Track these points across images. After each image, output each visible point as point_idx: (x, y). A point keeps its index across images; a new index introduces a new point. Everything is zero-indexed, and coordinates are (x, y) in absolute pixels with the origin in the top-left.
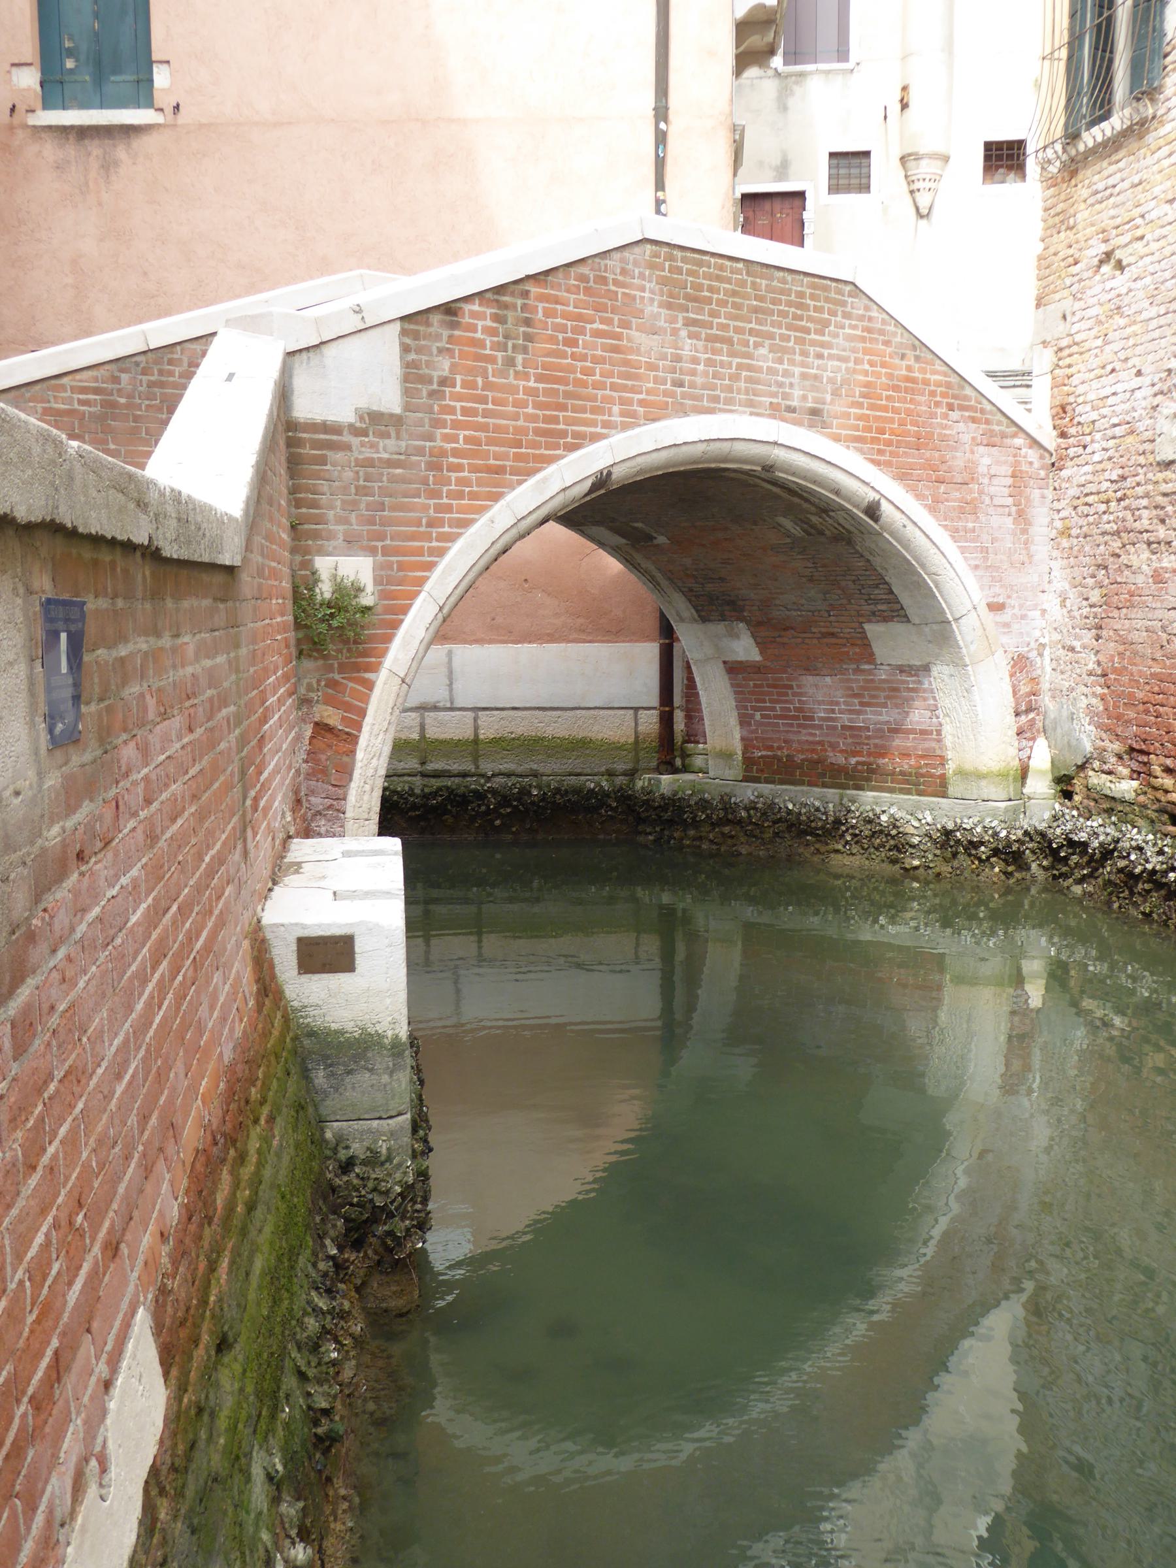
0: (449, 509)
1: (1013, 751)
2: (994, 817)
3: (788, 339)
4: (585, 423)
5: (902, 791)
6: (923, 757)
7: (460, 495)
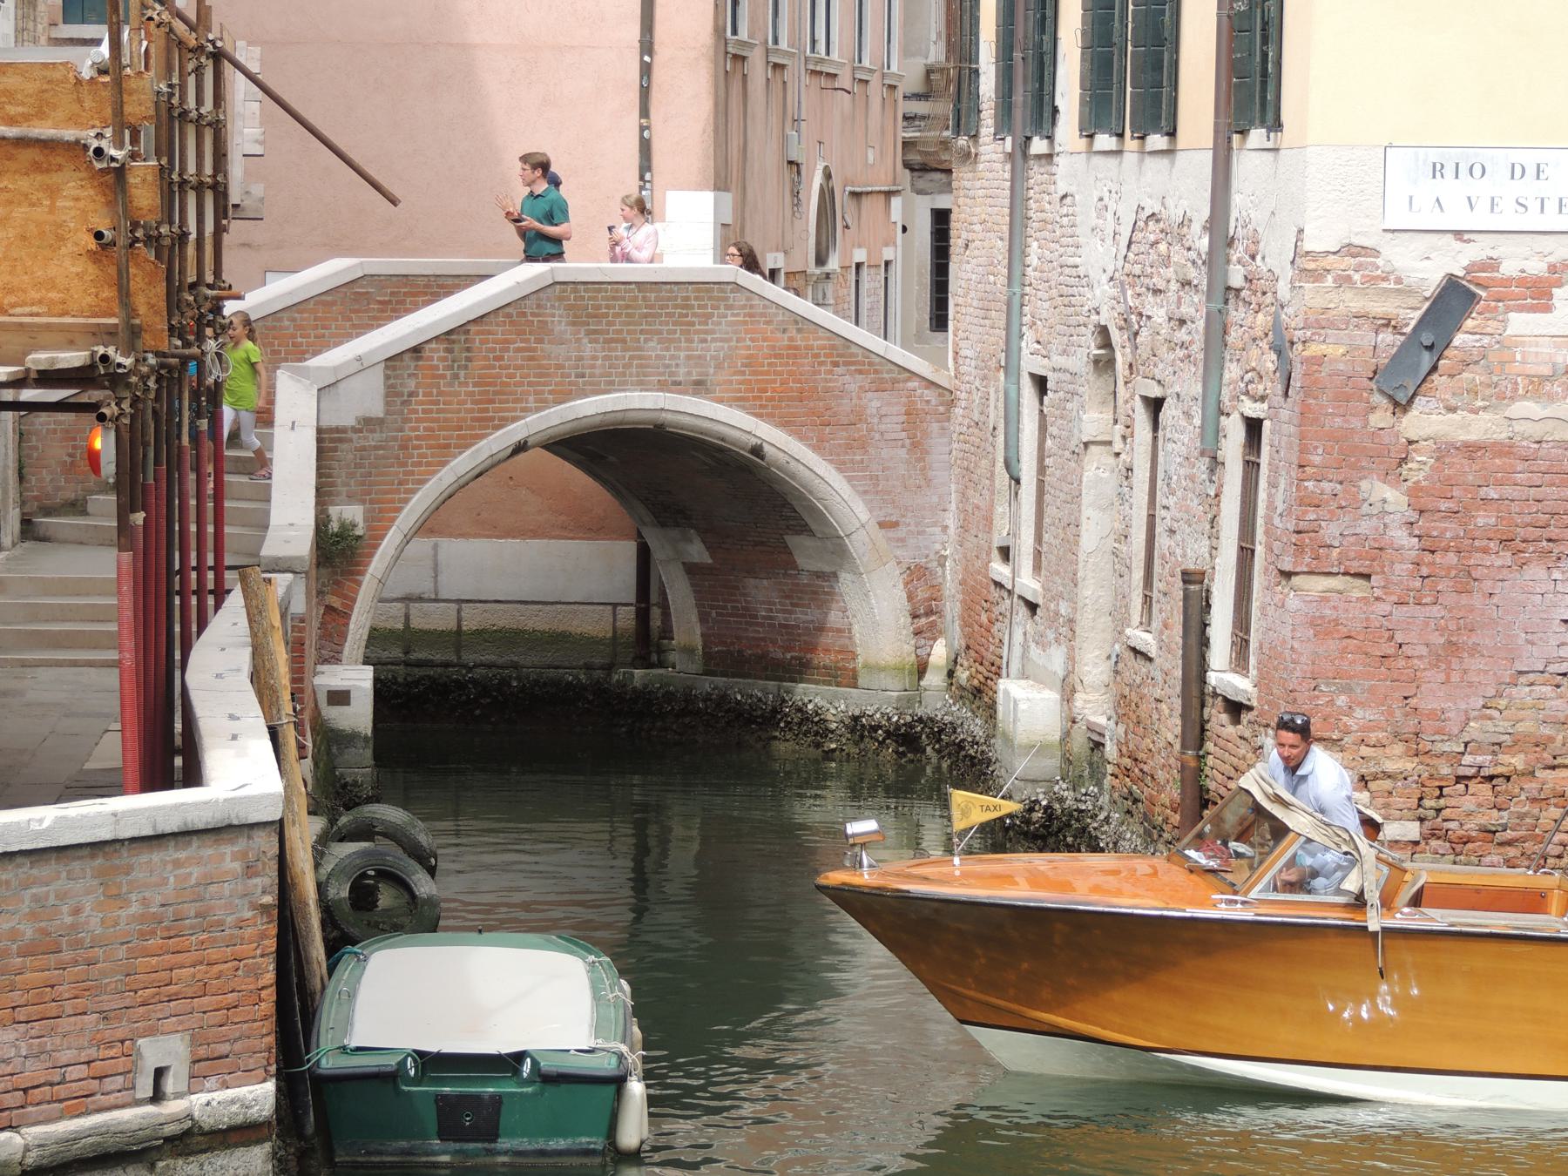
0: (412, 473)
1: (908, 648)
2: (889, 704)
3: (675, 332)
4: (508, 410)
5: (825, 683)
6: (840, 652)
7: (419, 464)
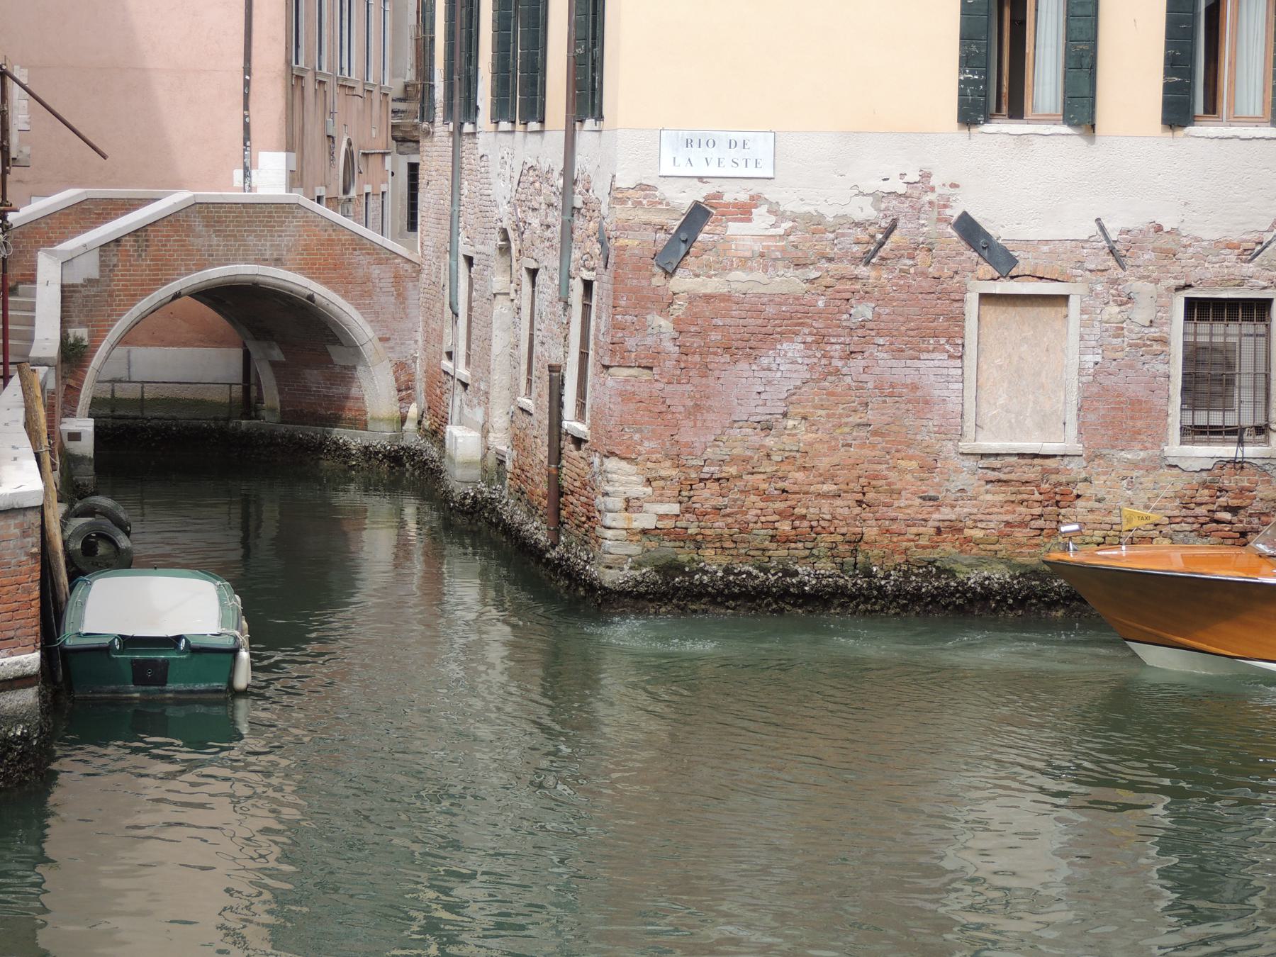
1: (396, 408)
